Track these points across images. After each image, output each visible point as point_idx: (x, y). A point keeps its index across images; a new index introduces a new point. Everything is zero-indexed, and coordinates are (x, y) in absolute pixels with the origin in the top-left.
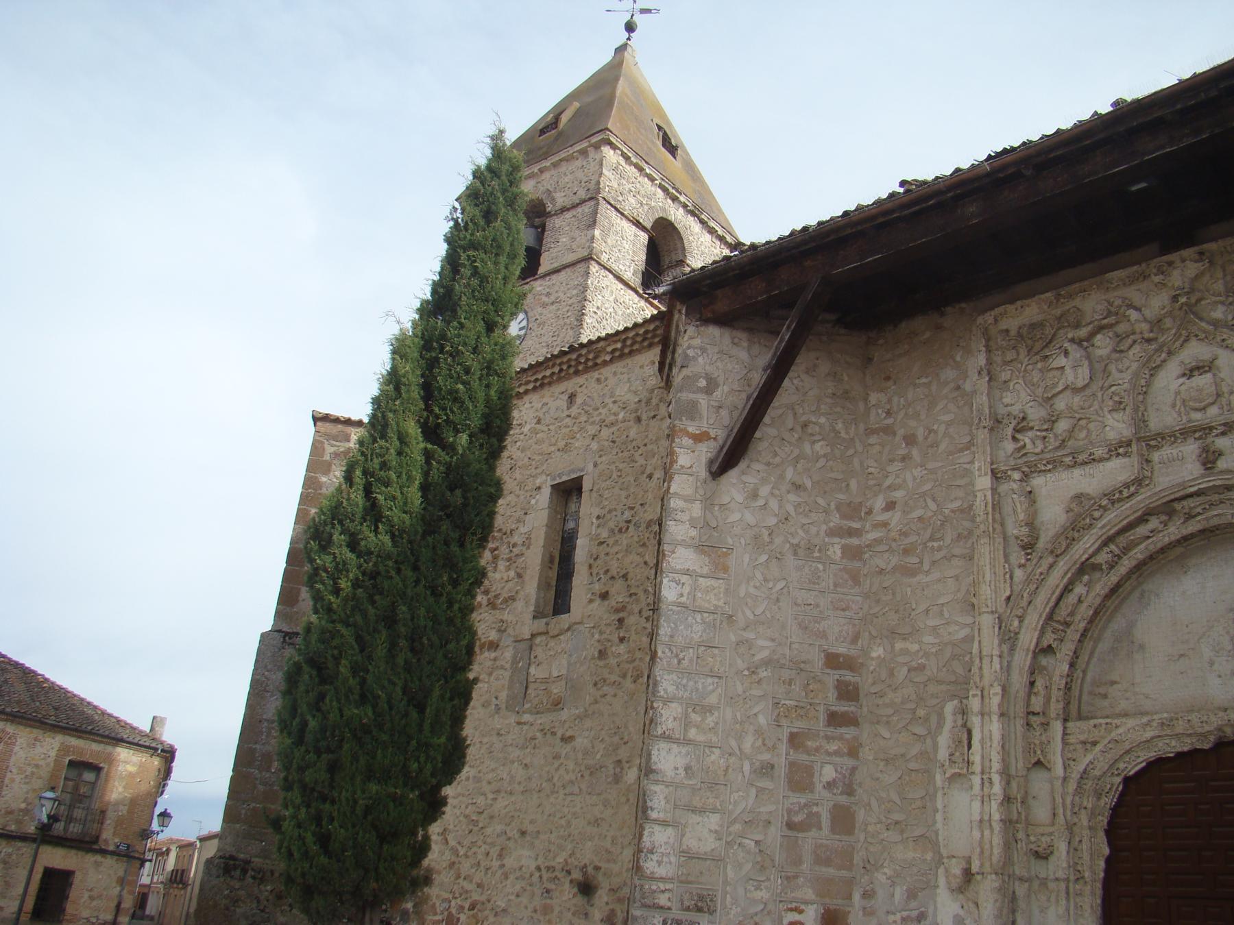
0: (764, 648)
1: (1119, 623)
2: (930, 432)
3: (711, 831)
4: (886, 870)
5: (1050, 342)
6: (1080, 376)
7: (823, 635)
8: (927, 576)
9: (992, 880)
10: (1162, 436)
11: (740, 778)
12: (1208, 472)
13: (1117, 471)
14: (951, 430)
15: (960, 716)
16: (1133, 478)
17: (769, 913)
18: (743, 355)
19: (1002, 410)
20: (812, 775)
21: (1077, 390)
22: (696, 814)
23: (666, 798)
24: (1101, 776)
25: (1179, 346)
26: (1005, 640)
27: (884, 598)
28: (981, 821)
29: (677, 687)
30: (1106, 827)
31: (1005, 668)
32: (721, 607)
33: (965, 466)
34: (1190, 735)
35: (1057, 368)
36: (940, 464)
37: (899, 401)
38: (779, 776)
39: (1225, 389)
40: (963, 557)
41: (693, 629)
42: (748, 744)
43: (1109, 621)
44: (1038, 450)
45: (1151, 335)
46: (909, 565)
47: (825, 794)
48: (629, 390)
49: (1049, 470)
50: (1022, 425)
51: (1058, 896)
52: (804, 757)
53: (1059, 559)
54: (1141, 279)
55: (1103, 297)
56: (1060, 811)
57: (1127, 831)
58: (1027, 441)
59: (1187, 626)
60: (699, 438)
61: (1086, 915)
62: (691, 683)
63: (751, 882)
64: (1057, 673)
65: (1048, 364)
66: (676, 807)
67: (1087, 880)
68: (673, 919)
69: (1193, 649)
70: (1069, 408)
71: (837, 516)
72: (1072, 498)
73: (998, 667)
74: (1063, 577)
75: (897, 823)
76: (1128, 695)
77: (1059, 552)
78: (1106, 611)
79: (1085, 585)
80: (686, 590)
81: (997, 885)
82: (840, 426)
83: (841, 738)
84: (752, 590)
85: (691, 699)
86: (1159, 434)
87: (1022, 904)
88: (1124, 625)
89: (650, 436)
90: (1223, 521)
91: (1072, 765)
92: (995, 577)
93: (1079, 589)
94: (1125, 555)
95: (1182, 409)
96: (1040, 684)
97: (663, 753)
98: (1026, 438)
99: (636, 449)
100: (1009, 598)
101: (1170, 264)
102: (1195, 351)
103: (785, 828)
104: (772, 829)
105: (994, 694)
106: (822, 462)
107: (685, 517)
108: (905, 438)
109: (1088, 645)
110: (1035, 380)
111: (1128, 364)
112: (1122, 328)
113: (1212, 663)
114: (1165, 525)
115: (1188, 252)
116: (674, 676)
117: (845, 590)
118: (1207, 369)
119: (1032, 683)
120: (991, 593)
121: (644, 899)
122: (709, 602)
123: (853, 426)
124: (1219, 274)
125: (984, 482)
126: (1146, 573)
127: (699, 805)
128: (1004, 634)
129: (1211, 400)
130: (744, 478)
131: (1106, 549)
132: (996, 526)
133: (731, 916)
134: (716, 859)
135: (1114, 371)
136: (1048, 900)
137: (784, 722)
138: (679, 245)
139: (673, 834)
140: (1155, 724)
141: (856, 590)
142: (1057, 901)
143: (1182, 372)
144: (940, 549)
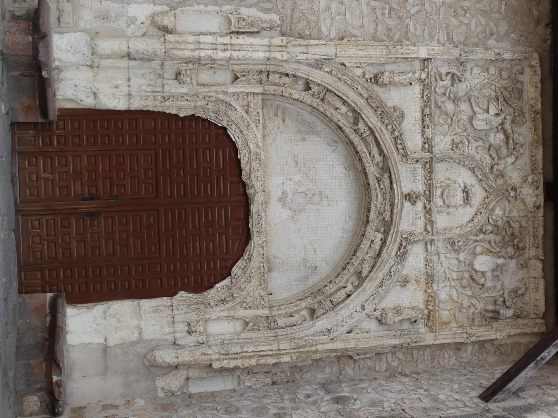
1: (319, 125)
6: (480, 123)
8: (366, 3)
9: (161, 49)
12: (404, 196)
14: (464, 28)
15: (269, 25)
16: (409, 153)
19: (469, 66)
24: (227, 115)
25: (484, 186)
26: (316, 62)
28: (199, 42)
30: (196, 115)
33: (437, 37)
34: (250, 170)
35: (488, 107)
36: (441, 17)
39: (451, 210)
40: (375, 32)
43: (322, 121)
45: (495, 170)
49: (423, 97)
50: (456, 80)
51: (153, 86)
53: (365, 100)
54: (533, 167)
55: (527, 142)
56: (206, 89)
57: (194, 126)
58: (445, 83)
59: (314, 167)
61: (142, 102)
64: (293, 91)
67: (164, 103)
69: (300, 169)
70: (461, 112)
72: (402, 112)
73: (299, 58)
74: (353, 101)
76: (276, 129)
77: (369, 101)
78: (328, 121)
79: (346, 113)
81: (158, 52)
86: (432, 171)
87: (147, 64)
88: (318, 129)
90: (373, 198)
91: (234, 97)
92: (360, 57)
93: (344, 109)
94: (361, 139)
95: (444, 184)
96: (287, 80)
98: (447, 82)
100: (344, 65)
101: (537, 188)
102: (478, 194)
105: (282, 55)
111: (480, 153)
112: (504, 151)
113: (290, 180)
114: (376, 164)
115: (541, 199)
118: (466, 201)
119: (287, 75)
124: (521, 214)
125: (423, 53)
126: (348, 147)
128: (320, 61)
129: (447, 202)
131: (367, 129)
132: (393, 59)
136: (150, 80)
140: (258, 150)
143: (467, 186)
144: (383, 14)
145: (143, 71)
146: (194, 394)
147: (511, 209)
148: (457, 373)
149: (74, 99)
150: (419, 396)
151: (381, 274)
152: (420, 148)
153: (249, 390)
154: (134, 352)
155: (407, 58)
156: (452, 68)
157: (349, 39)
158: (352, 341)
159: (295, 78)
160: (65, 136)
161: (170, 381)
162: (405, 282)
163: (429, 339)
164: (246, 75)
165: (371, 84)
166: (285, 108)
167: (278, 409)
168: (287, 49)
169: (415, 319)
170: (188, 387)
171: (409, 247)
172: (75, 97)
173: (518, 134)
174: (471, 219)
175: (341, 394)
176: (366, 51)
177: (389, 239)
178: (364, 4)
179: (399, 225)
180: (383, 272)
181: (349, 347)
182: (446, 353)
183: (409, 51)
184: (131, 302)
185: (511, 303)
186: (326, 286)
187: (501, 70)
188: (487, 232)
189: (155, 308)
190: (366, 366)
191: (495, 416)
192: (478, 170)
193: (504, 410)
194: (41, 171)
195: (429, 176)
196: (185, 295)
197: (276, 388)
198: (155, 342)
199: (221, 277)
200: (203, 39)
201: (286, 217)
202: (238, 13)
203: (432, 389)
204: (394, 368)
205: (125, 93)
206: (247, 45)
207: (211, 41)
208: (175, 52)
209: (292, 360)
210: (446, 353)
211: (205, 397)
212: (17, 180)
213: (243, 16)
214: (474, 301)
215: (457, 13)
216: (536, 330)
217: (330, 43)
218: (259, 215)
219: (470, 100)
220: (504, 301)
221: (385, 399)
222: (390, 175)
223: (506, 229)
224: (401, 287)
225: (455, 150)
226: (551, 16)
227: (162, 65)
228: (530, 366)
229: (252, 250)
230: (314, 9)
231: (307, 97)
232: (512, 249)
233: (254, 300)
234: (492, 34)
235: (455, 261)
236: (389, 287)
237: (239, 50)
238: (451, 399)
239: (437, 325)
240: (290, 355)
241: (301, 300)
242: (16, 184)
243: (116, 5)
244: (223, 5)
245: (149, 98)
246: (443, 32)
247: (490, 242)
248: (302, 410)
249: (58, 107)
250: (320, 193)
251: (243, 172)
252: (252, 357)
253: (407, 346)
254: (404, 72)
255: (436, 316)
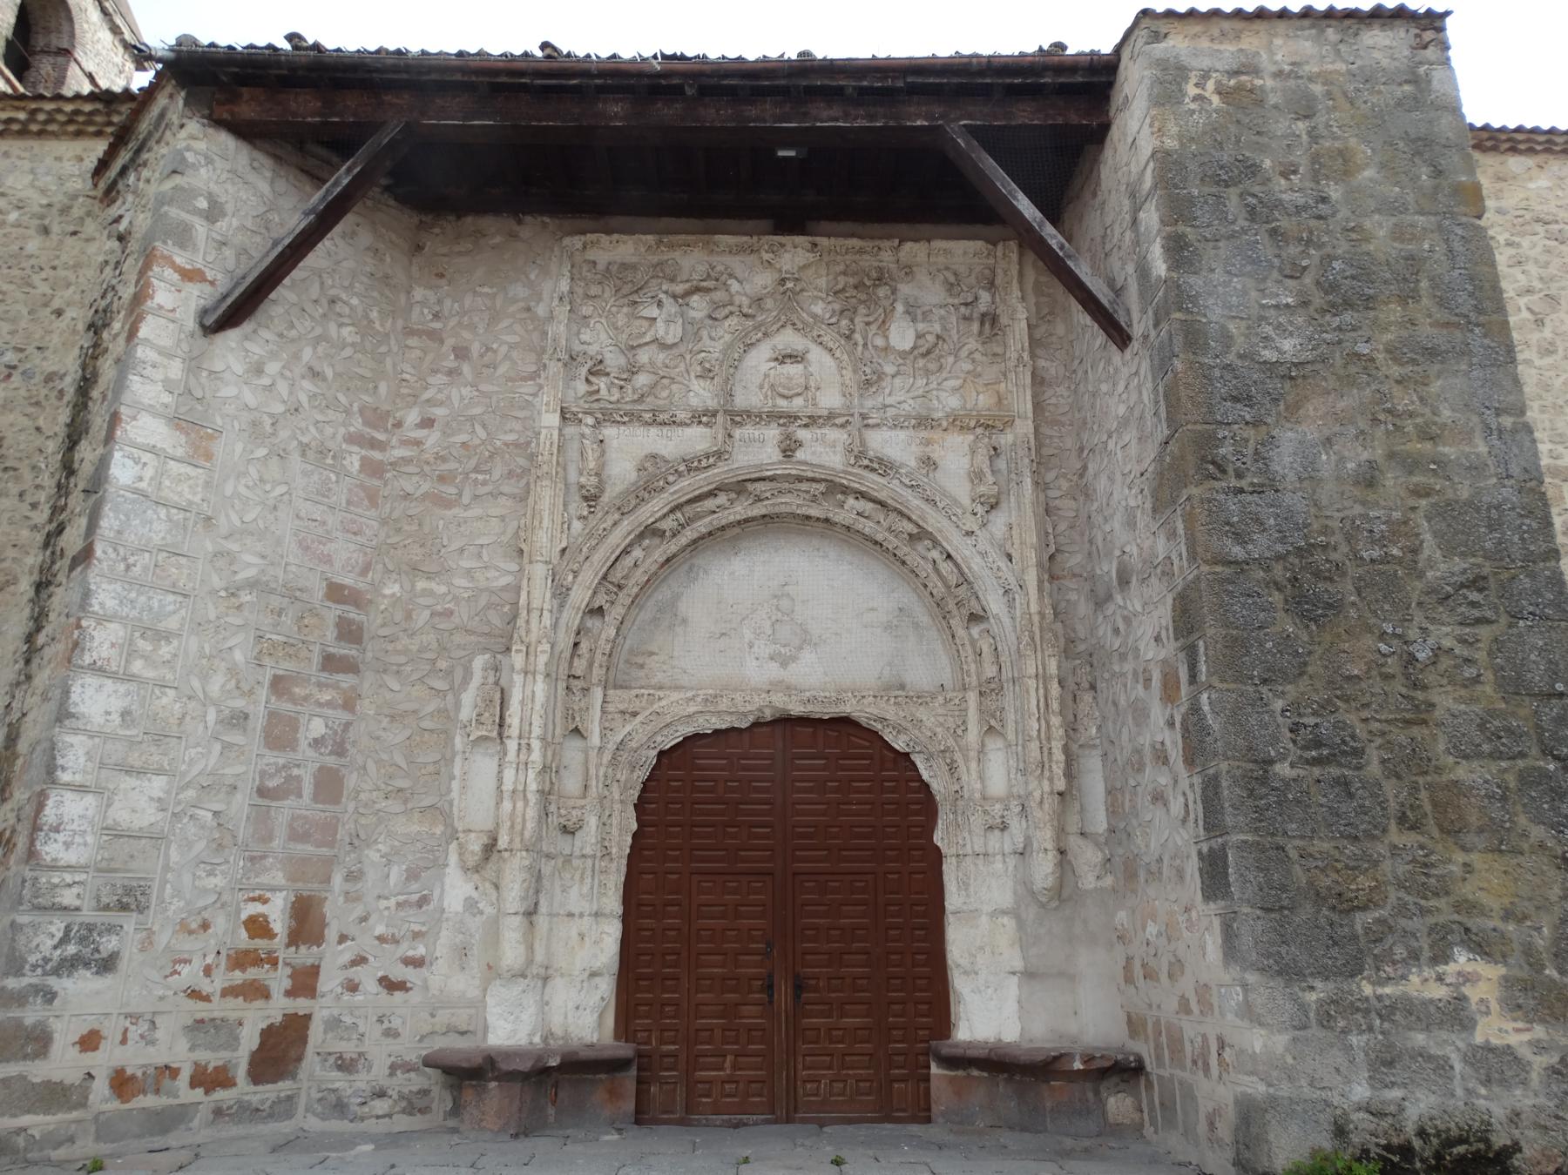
0: (250, 565)
1: (663, 594)
3: (151, 799)
4: (380, 846)
5: (641, 288)
6: (671, 333)
7: (327, 560)
10: (748, 413)
11: (201, 727)
13: (696, 439)
15: (492, 673)
17: (223, 906)
18: (264, 187)
20: (296, 730)
21: (664, 346)
22: (131, 776)
23: (87, 753)
27: (407, 528)
28: (514, 792)
29: (121, 602)
32: (198, 505)
34: (732, 713)
36: (496, 389)
38: (254, 729)
40: (513, 496)
41: (157, 528)
42: (216, 685)
44: (613, 399)
47: (311, 753)
48: (32, 185)
51: (583, 874)
52: (289, 706)
55: (706, 258)
58: (603, 386)
60: (190, 275)
62: (143, 599)
63: (202, 866)
64: (603, 636)
66: (102, 766)
68: (81, 924)
70: (652, 363)
71: (360, 420)
73: (548, 623)
75: (400, 790)
76: (665, 667)
80: (149, 473)
82: (374, 315)
83: (336, 686)
84: (242, 490)
85: (140, 620)
87: (545, 882)
89: (64, 258)
93: (637, 553)
96: (584, 647)
97: (90, 691)
98: (601, 383)
99: (37, 269)
100: (564, 550)
101: (782, 245)
102: (789, 339)
103: (255, 795)
104: (239, 796)
106: (348, 352)
107: (158, 375)
108: (454, 349)
110: (620, 324)
112: (719, 296)
113: (751, 646)
116: (118, 587)
117: (360, 511)
119: (576, 645)
120: (546, 541)
121: (37, 897)
122: (180, 494)
123: (390, 320)
127: (138, 764)
129: (799, 390)
130: (248, 345)
131: (672, 516)
133: (170, 913)
134: (157, 838)
136: (572, 878)
137: (267, 661)
138: (65, 27)
139: (94, 804)
140: (699, 699)
141: (373, 513)
142: (582, 878)
143: (774, 356)
144: (484, 483)
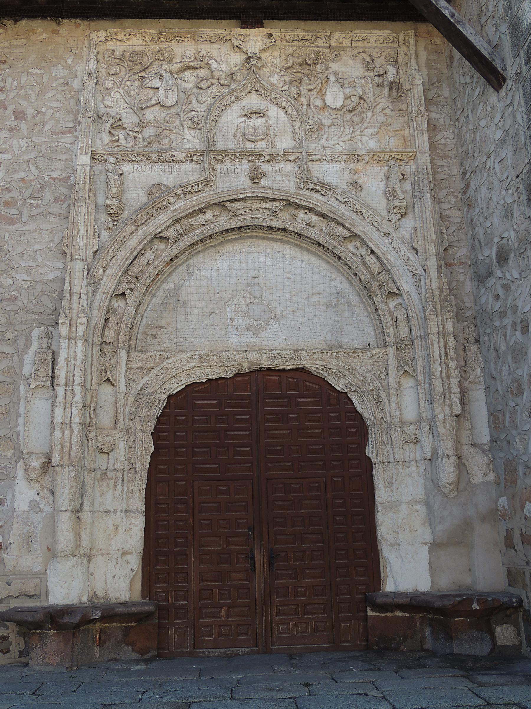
1: (169, 285)
2: (38, 113)
6: (170, 96)
9: (69, 471)
10: (226, 153)
12: (254, 185)
14: (58, 115)
19: (102, 110)
25: (244, 94)
30: (153, 431)
31: (89, 304)
33: (66, 145)
36: (44, 140)
37: (12, 83)
46: (9, 215)
51: (115, 482)
58: (121, 136)
61: (136, 495)
65: (145, 83)
67: (137, 470)
76: (172, 337)
77: (140, 223)
86: (226, 151)
87: (88, 488)
92: (87, 234)
93: (149, 255)
95: (241, 139)
96: (113, 320)
98: (121, 135)
105: (80, 324)
109: (148, 297)
112: (202, 73)
119: (106, 320)
125: (86, 159)
129: (262, 137)
135: (194, 101)
144: (38, 206)
145: (98, 494)
146: (491, 436)
147: (272, 65)
148: (463, 128)
149: (130, 579)
150: (496, 162)
151: (347, 214)
152: (198, 166)
153: (487, 371)
154: (440, 509)
155: (90, 178)
156: (105, 129)
157: (65, 245)
158: (427, 248)
159: (111, 311)
160: (175, 591)
161: (475, 465)
162: (357, 185)
163: (424, 159)
164: (105, 369)
165: (119, 221)
166: (147, 326)
167: (516, 330)
168: (74, 318)
169: (401, 175)
170: (482, 444)
171: (315, 180)
172: (127, 577)
173: (184, 57)
174: (282, 110)
175: (494, 257)
176: (79, 225)
177: (306, 204)
178: (24, 229)
179: (288, 192)
180: (344, 212)
181: (434, 251)
182: (439, 142)
183: (82, 175)
184: (379, 513)
185: (381, 68)
186: (360, 279)
187: (109, 74)
188: (298, 92)
189: (386, 483)
190: (455, 234)
191: (526, 63)
192: (226, 100)
193: (516, 55)
194: (218, 621)
195: (230, 156)
196: (370, 448)
197: (484, 338)
198: (428, 483)
199: (348, 405)
200: (58, 419)
201: (278, 326)
202: (29, 377)
203: (487, 150)
204: (457, 201)
205: (124, 516)
206: (67, 365)
207: (62, 410)
208: (73, 454)
209: (450, 318)
210: (439, 142)
211: (495, 423)
212: (229, 651)
213: (33, 370)
214: (379, 109)
215: (40, 123)
216: (412, 42)
217: (69, 267)
218: (275, 357)
219: (142, 108)
220: (379, 76)
221: (502, 202)
222: (228, 201)
223: (294, 72)
224: (363, 190)
225: (202, 125)
226: (49, 18)
227: (90, 471)
228: (462, 30)
229: (316, 366)
230: (28, 287)
231: (134, 297)
232: (318, 66)
233: (376, 365)
234: (67, 84)
235: (332, 130)
236: (362, 204)
237: (74, 375)
238: (500, 124)
239: (407, 150)
240: (445, 320)
241: (376, 309)
242: (233, 651)
243: (15, 526)
244: (19, 396)
245: (131, 488)
246: (61, 138)
247: (310, 90)
248: (517, 300)
249: (140, 599)
250: (249, 286)
251: (223, 376)
252: (447, 366)
253: (432, 185)
254: (107, 183)
255: (396, 152)
